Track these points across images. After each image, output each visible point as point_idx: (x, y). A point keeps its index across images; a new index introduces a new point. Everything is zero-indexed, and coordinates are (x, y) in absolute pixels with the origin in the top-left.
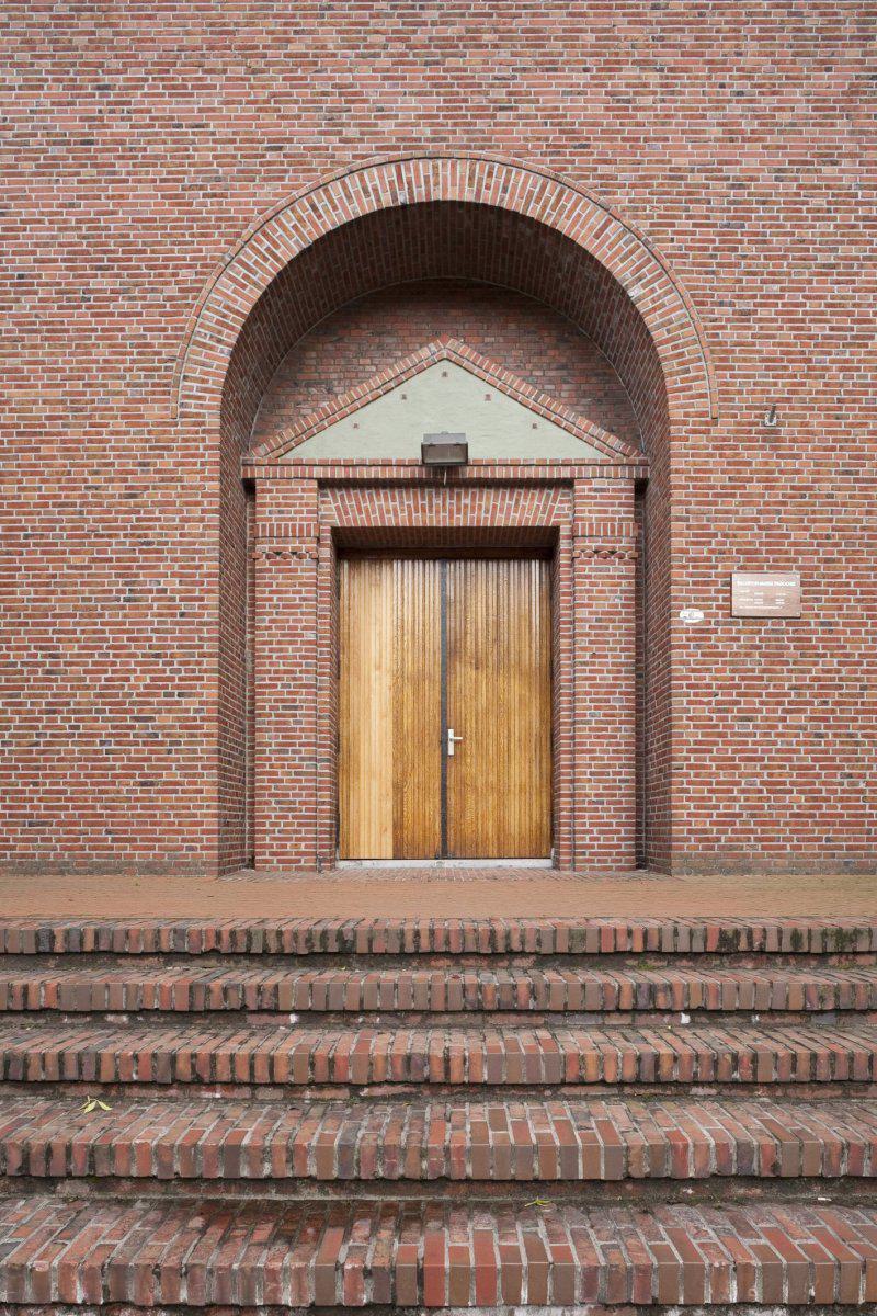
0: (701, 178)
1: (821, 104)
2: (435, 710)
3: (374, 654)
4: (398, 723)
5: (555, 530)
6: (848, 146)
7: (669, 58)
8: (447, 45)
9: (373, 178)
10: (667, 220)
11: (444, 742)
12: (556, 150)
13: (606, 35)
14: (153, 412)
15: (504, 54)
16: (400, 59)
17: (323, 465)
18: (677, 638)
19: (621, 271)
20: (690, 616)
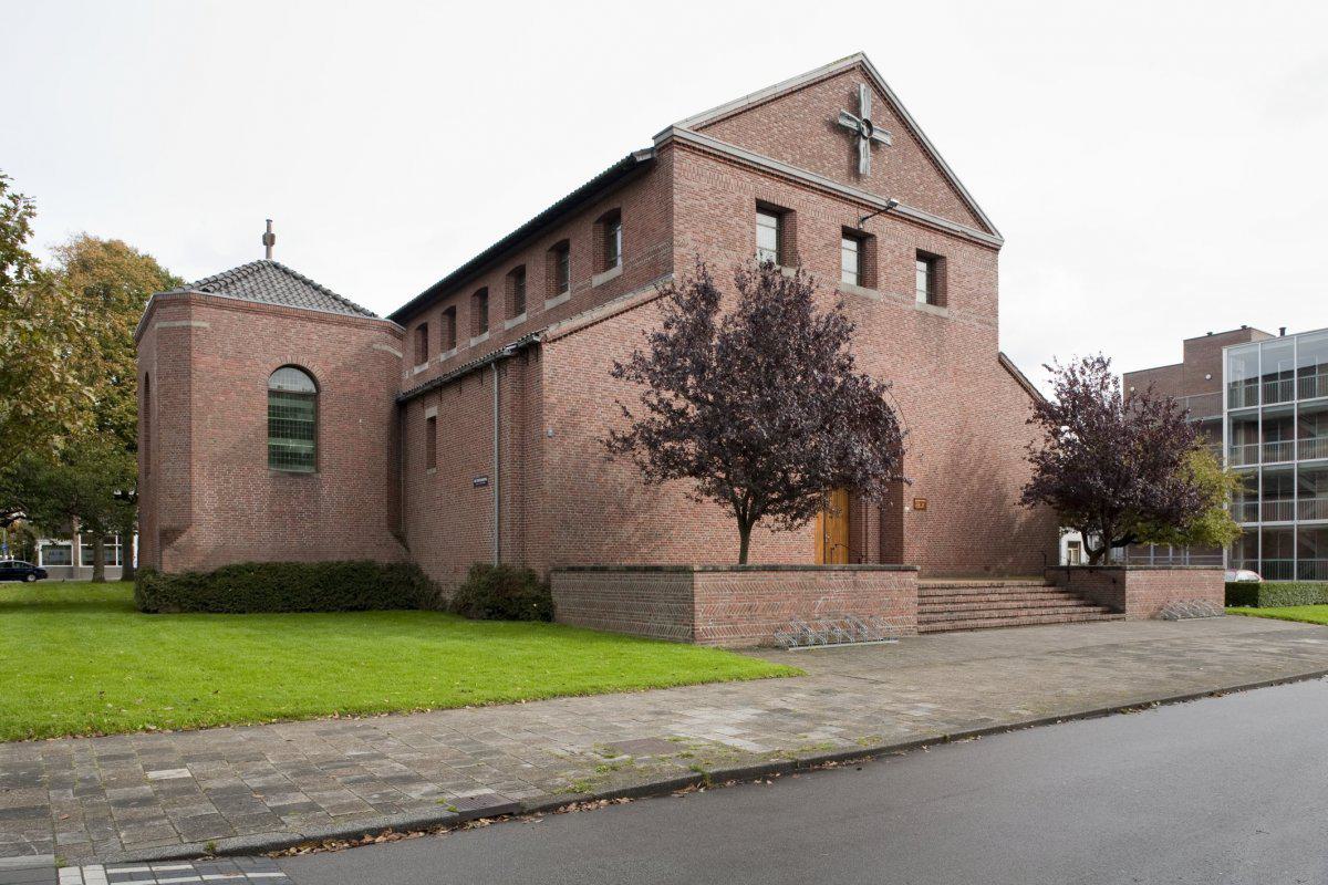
20: (907, 509)
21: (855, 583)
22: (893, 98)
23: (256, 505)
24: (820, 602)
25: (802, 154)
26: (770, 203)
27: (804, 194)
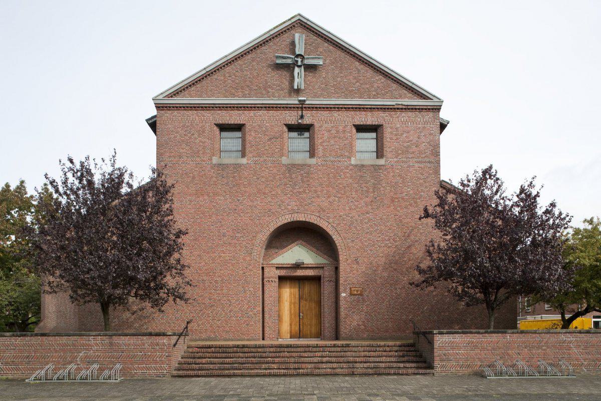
0: (345, 216)
1: (366, 203)
2: (298, 309)
3: (286, 299)
4: (290, 312)
5: (321, 276)
6: (371, 211)
7: (339, 195)
8: (300, 193)
9: (287, 217)
10: (339, 224)
11: (300, 316)
12: (319, 212)
13: (328, 191)
14: (248, 258)
15: (310, 194)
16: (291, 195)
17: (277, 264)
18: (341, 299)
19: (330, 233)
20: (343, 295)
21: (111, 344)
22: (327, 34)
23: (69, 309)
24: (81, 354)
25: (251, 89)
26: (228, 124)
27: (252, 113)
